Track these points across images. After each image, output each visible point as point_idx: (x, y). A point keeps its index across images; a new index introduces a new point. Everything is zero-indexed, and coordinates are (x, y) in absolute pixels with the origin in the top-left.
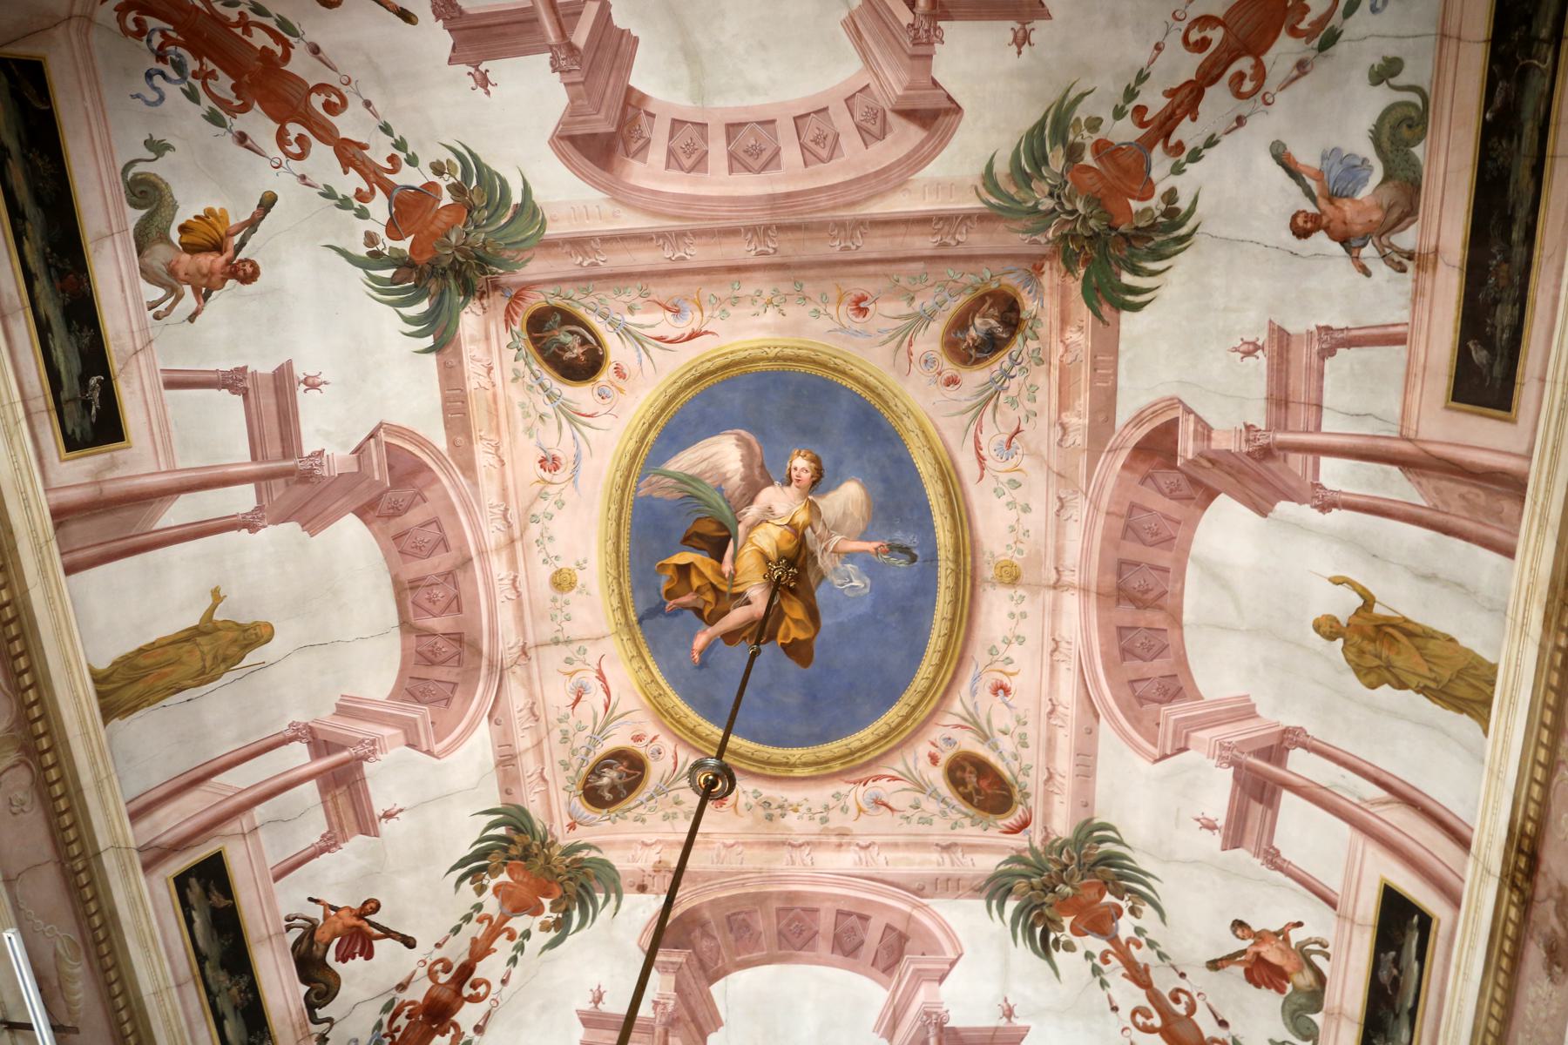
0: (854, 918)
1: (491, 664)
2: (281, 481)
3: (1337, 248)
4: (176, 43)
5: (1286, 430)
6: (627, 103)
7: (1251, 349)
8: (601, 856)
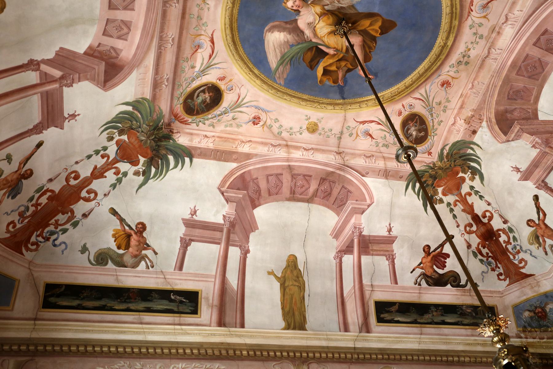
0: (542, 38)
1: (340, 169)
2: (232, 235)
4: (42, 232)
6: (92, 55)
8: (450, 145)
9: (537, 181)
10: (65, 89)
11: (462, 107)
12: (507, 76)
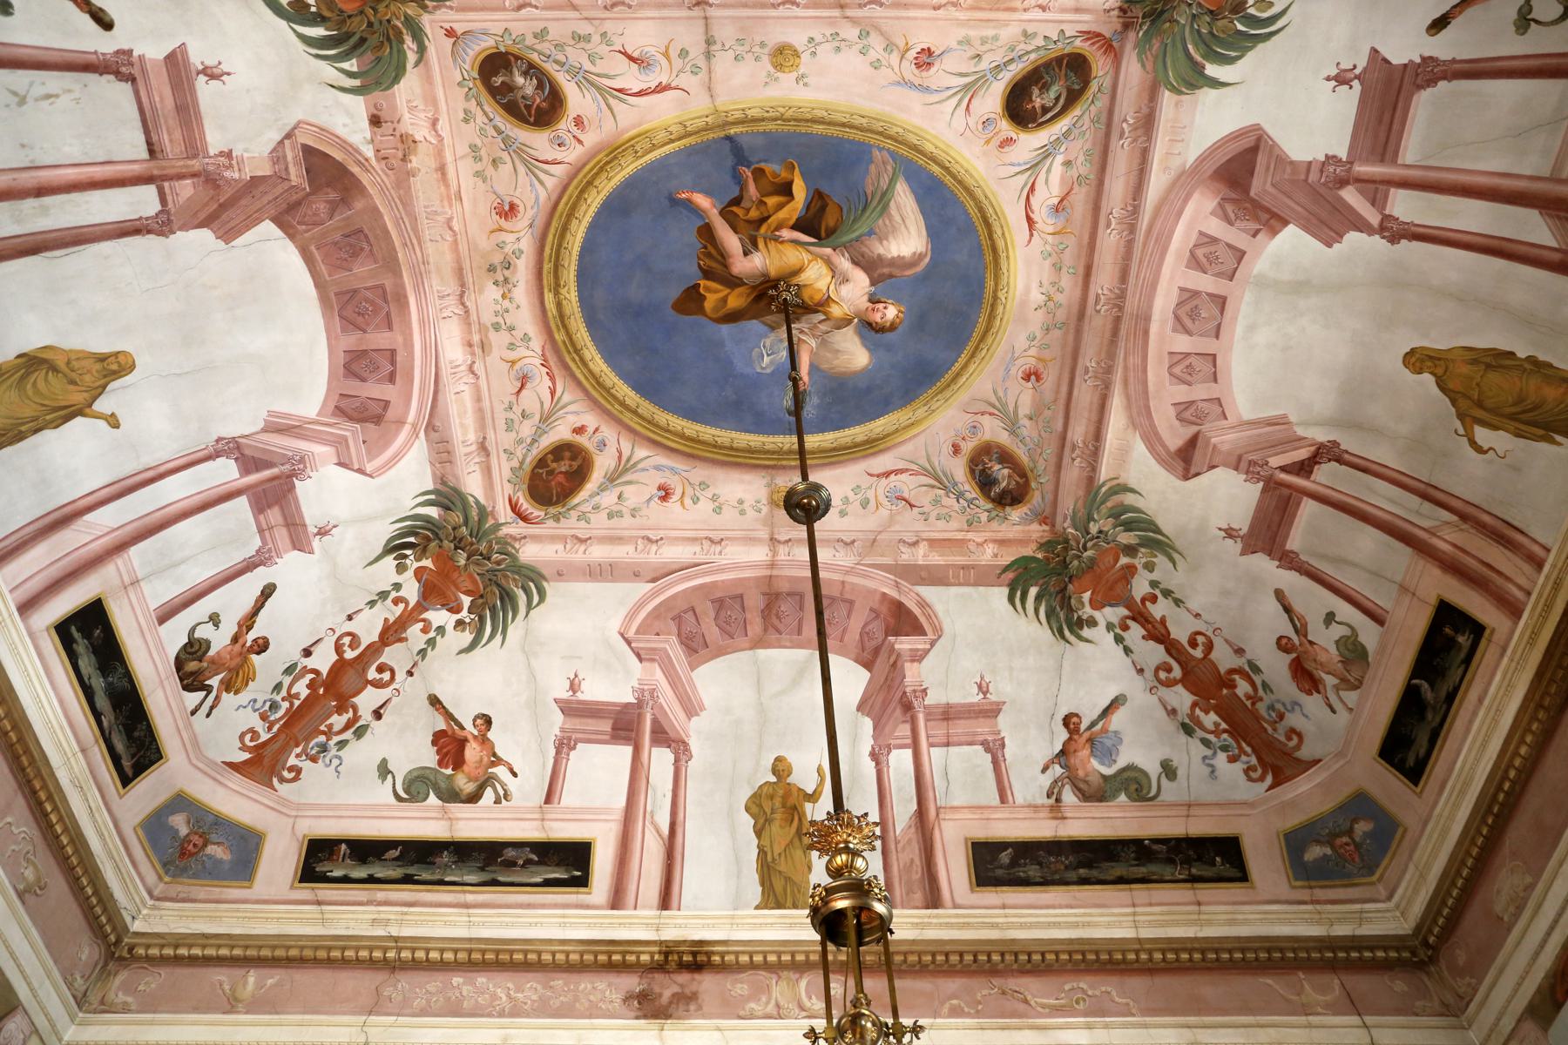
0: (390, 368)
3: (1058, 747)
5: (927, 720)
7: (983, 689)
8: (409, 66)
9: (143, 71)
10: (1343, 155)
11: (442, 169)
12: (397, 273)
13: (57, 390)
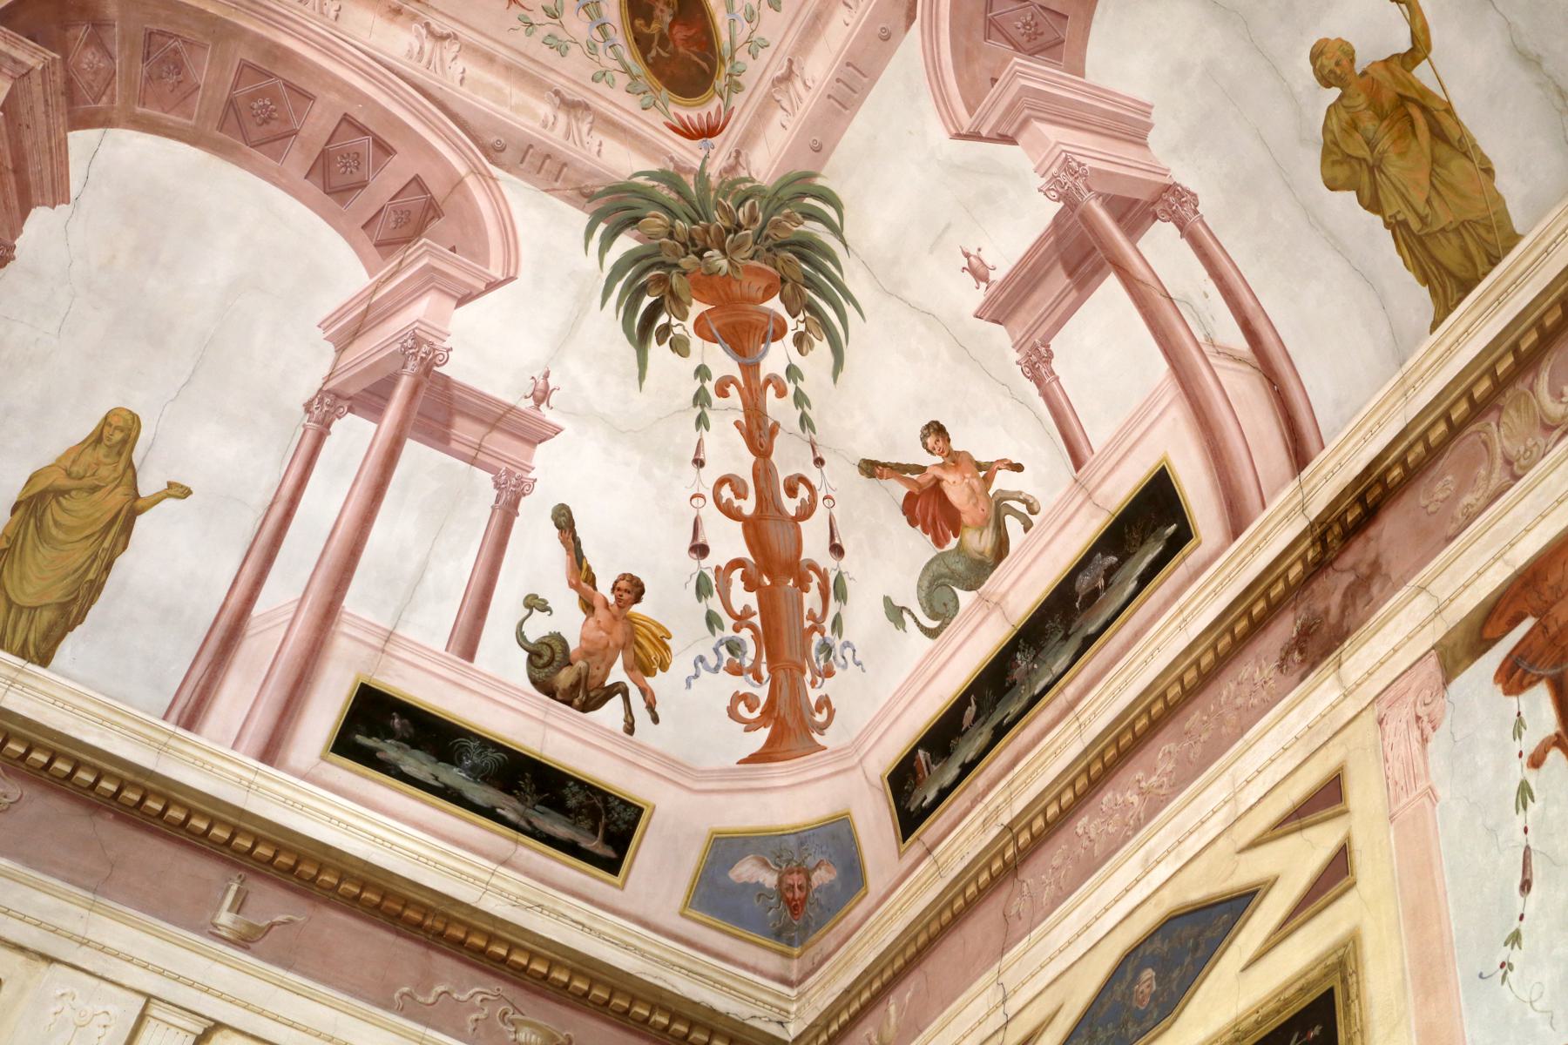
12: (238, 32)
13: (81, 511)
